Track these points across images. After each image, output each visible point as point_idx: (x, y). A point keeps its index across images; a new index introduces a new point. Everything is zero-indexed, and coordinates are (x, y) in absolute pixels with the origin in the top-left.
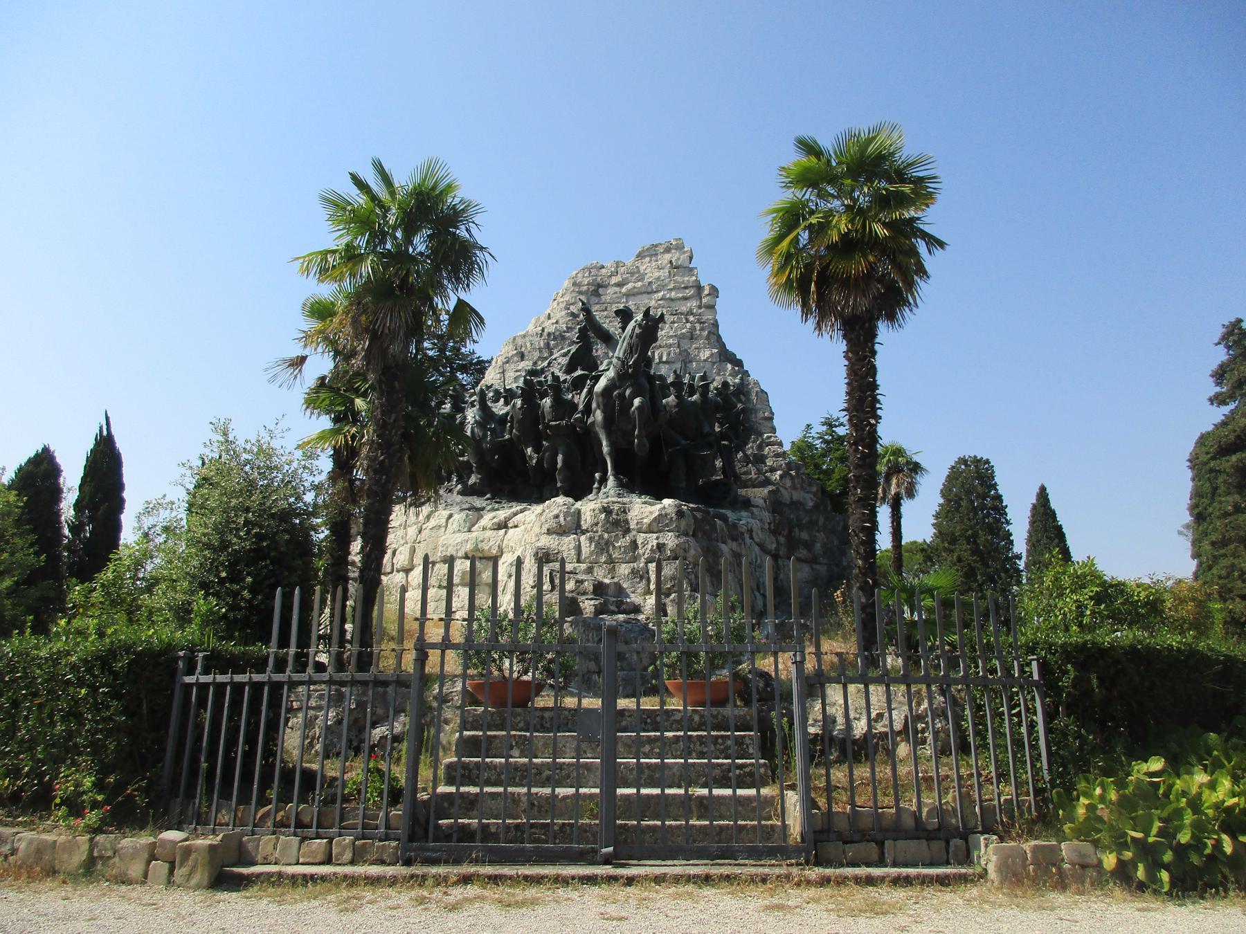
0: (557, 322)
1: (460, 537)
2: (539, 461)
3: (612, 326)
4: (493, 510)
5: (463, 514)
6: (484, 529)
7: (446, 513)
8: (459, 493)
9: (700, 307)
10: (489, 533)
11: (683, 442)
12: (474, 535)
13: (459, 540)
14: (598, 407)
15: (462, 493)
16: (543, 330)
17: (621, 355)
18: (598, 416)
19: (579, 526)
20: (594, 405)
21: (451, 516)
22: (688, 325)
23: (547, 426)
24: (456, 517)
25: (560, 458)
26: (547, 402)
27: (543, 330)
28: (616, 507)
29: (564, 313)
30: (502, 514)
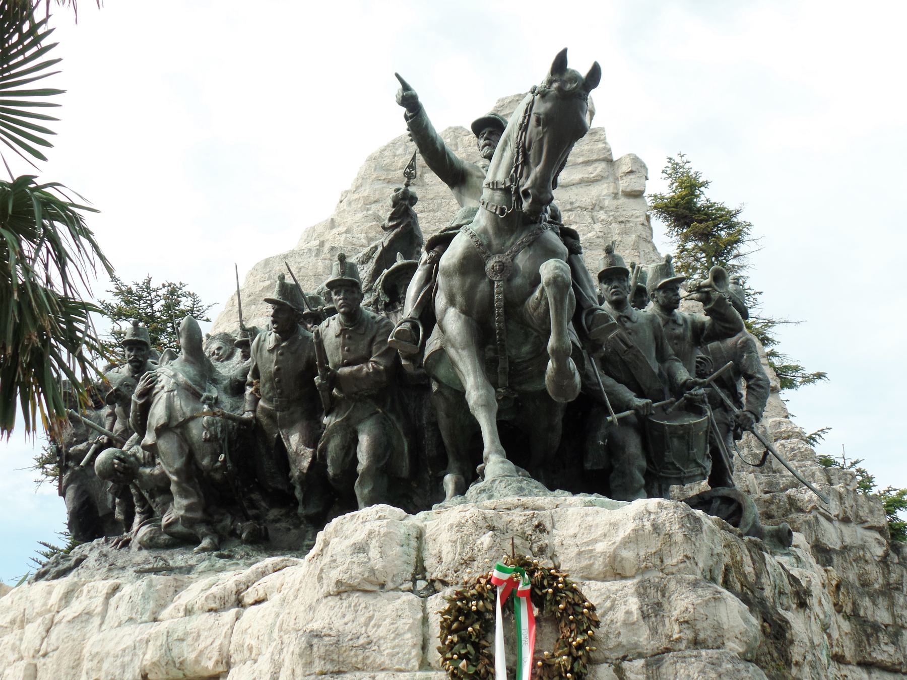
0: (348, 231)
1: (130, 635)
2: (318, 463)
3: (465, 150)
4: (212, 569)
5: (142, 584)
6: (189, 612)
7: (104, 586)
8: (143, 546)
9: (615, 196)
10: (201, 620)
11: (639, 402)
12: (162, 627)
13: (128, 642)
14: (451, 301)
15: (150, 544)
16: (322, 244)
17: (501, 177)
18: (452, 321)
19: (420, 570)
20: (440, 301)
21: (116, 589)
22: (598, 227)
23: (333, 380)
24: (127, 590)
25: (364, 441)
26: (331, 328)
27: (322, 244)
28: (518, 517)
29: (360, 215)
30: (230, 577)
